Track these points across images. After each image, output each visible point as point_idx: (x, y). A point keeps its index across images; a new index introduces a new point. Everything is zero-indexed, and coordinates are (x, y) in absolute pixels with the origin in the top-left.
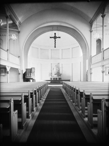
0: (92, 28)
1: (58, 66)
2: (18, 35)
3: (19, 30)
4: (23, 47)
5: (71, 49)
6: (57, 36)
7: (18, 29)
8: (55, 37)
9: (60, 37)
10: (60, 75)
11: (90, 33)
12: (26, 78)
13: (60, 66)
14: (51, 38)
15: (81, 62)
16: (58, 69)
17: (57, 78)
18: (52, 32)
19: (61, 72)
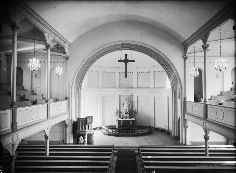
0: (187, 53)
1: (130, 101)
2: (65, 62)
3: (68, 54)
4: (73, 80)
5: (152, 73)
6: (129, 58)
7: (66, 53)
8: (126, 61)
9: (133, 61)
10: (135, 114)
11: (183, 60)
12: (77, 132)
13: (135, 99)
14: (119, 61)
15: (168, 98)
16: (130, 105)
17: (129, 121)
18: (120, 51)
19: (136, 110)
